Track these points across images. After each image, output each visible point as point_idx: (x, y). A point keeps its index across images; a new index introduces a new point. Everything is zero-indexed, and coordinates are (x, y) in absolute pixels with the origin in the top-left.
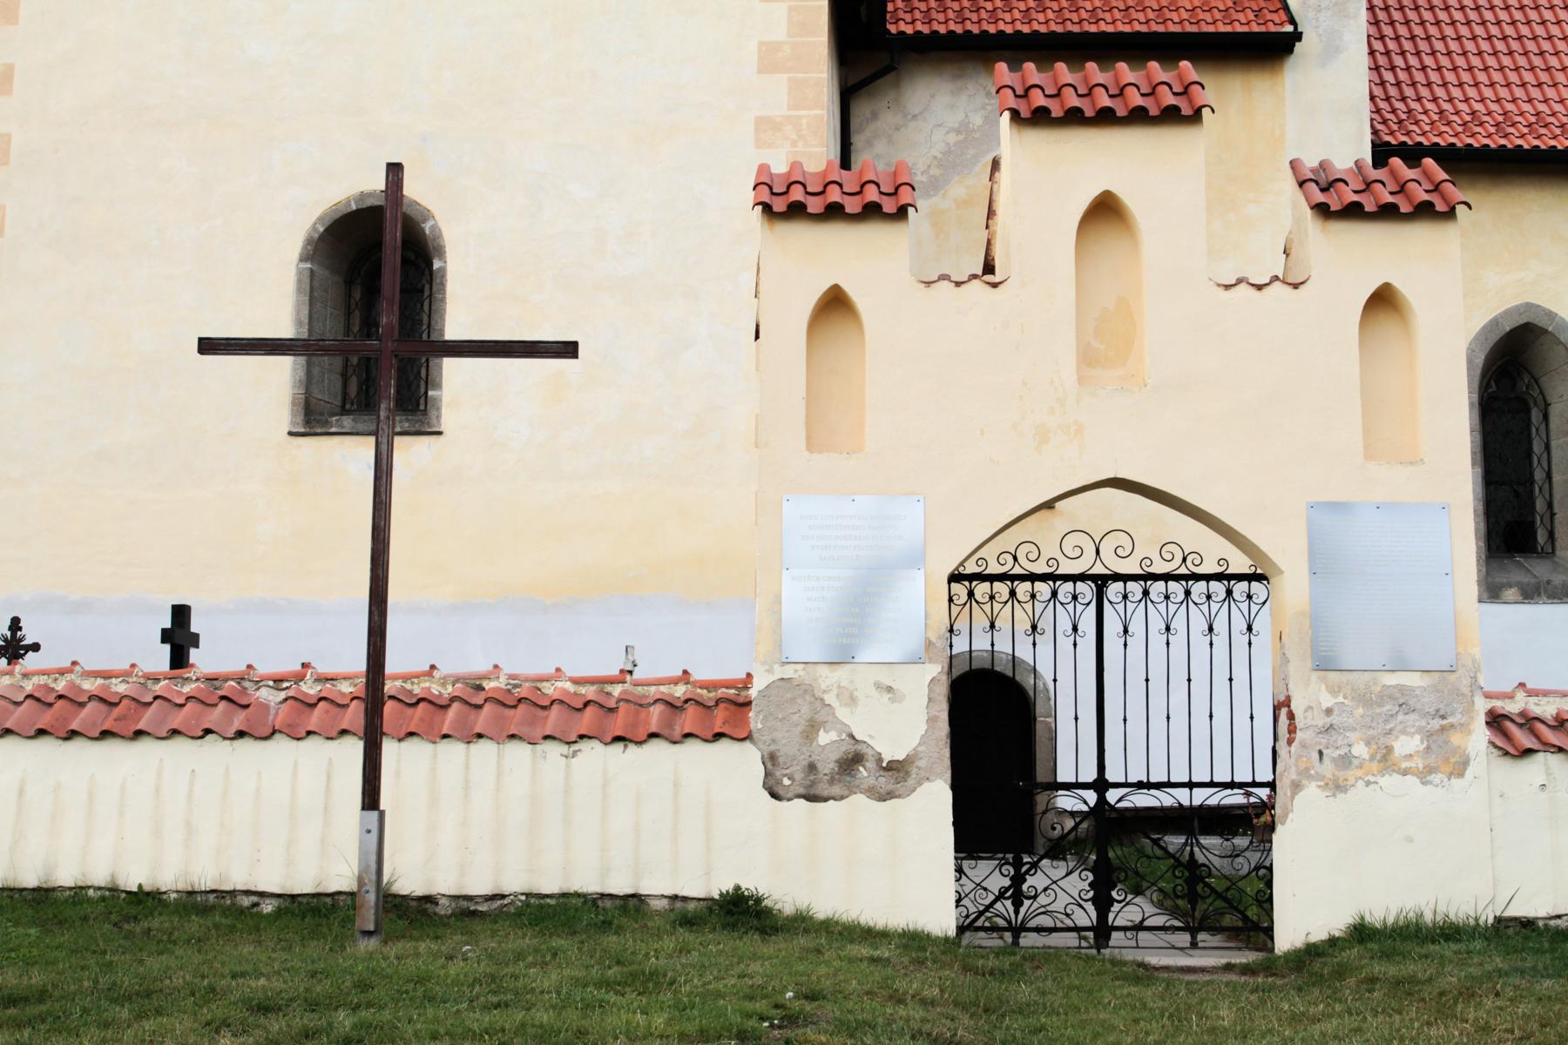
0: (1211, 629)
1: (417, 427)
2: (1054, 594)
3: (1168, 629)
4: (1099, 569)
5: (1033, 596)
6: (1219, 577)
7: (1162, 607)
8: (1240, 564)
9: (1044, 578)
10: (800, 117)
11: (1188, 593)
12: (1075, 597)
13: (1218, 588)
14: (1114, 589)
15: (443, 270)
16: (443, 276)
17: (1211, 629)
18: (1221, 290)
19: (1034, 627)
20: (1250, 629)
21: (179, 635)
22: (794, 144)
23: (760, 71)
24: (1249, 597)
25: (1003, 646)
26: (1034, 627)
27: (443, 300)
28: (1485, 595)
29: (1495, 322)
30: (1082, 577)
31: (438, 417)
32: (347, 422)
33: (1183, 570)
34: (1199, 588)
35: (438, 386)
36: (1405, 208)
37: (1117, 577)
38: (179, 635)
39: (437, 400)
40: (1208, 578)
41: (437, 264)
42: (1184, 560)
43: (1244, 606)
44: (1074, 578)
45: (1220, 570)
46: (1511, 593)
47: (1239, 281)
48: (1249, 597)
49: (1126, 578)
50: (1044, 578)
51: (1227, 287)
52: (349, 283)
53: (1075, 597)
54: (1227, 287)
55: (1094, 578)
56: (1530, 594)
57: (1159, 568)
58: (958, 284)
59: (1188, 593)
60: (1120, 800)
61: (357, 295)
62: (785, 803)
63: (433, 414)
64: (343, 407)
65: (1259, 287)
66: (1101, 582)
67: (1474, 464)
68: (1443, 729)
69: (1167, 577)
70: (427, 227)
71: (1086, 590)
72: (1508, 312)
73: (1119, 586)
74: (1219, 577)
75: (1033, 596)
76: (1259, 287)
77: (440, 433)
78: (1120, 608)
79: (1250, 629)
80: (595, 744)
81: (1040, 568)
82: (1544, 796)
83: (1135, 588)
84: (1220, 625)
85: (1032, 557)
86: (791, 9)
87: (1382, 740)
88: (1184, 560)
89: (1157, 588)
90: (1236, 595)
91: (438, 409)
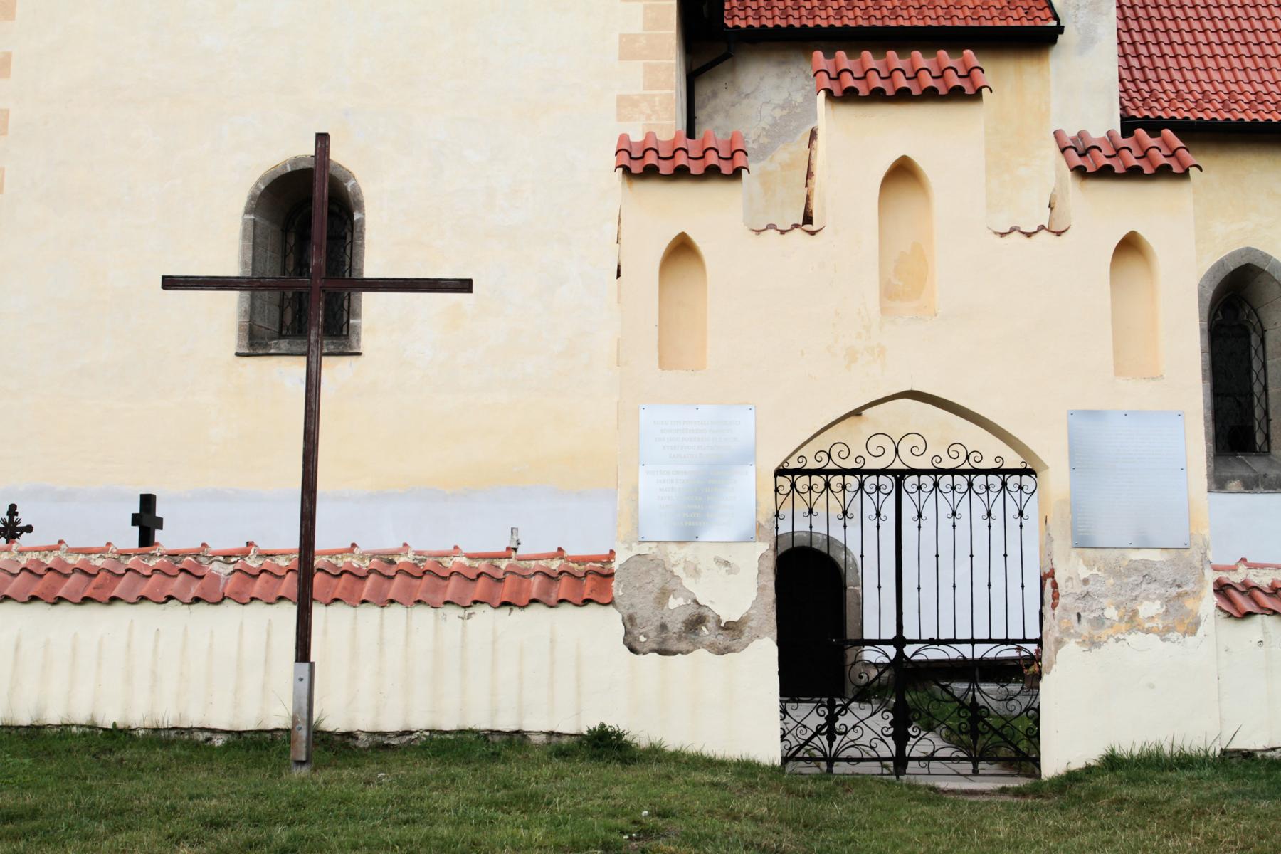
0: (989, 514)
1: (341, 349)
2: (861, 485)
3: (954, 514)
4: (898, 465)
5: (844, 487)
6: (996, 472)
7: (949, 496)
8: (1013, 461)
9: (853, 472)
10: (654, 96)
11: (970, 485)
12: (878, 488)
13: (995, 480)
14: (910, 481)
15: (362, 221)
16: (362, 226)
17: (989, 514)
18: (997, 237)
19: (845, 513)
20: (1021, 514)
21: (147, 519)
22: (649, 117)
23: (621, 58)
24: (1021, 488)
25: (819, 528)
26: (845, 513)
27: (362, 245)
28: (1213, 487)
29: (1221, 263)
30: (884, 472)
31: (358, 341)
32: (284, 345)
33: (966, 466)
34: (979, 480)
35: (358, 315)
36: (1148, 170)
37: (913, 472)
38: (147, 519)
39: (357, 327)
40: (987, 472)
41: (357, 216)
42: (968, 457)
43: (1017, 495)
44: (877, 473)
45: (996, 466)
46: (1234, 485)
47: (1013, 230)
48: (1021, 488)
49: (920, 472)
50: (853, 472)
51: (1003, 235)
52: (285, 232)
53: (878, 488)
54: (1003, 235)
55: (894, 472)
56: (1250, 485)
57: (947, 464)
58: (783, 232)
59: (970, 485)
60: (915, 654)
61: (292, 241)
62: (641, 656)
63: (353, 338)
64: (280, 332)
65: (1029, 235)
66: (899, 476)
67: (1204, 379)
68: (1179, 596)
69: (953, 472)
70: (349, 186)
71: (887, 482)
72: (1232, 255)
73: (914, 479)
74: (996, 472)
75: (844, 487)
76: (1029, 235)
77: (359, 354)
78: (915, 496)
79: (1021, 514)
80: (486, 608)
81: (850, 464)
82: (1261, 650)
83: (927, 480)
84: (997, 511)
85: (843, 455)
86: (646, 7)
87: (1129, 605)
88: (968, 457)
89: (945, 480)
90: (1010, 486)
91: (358, 334)
